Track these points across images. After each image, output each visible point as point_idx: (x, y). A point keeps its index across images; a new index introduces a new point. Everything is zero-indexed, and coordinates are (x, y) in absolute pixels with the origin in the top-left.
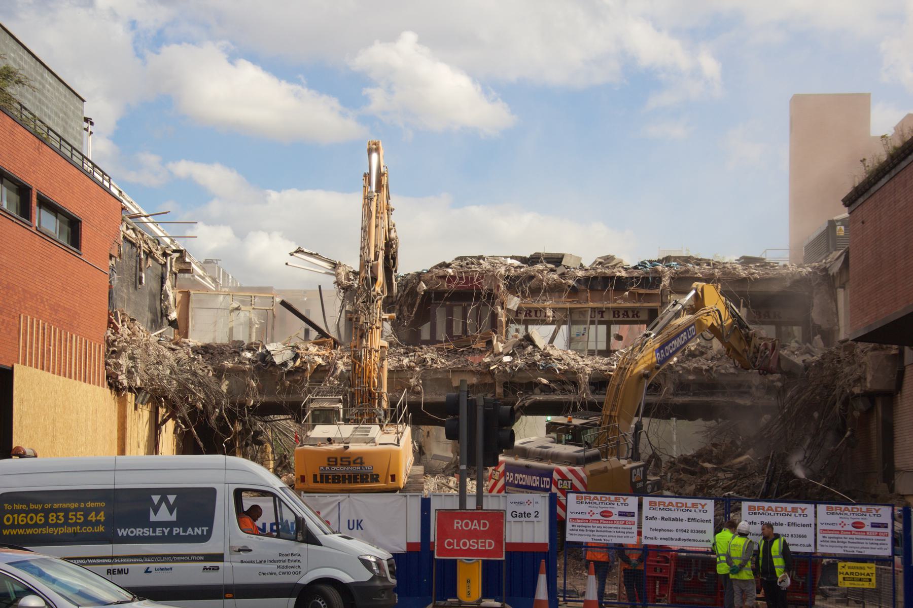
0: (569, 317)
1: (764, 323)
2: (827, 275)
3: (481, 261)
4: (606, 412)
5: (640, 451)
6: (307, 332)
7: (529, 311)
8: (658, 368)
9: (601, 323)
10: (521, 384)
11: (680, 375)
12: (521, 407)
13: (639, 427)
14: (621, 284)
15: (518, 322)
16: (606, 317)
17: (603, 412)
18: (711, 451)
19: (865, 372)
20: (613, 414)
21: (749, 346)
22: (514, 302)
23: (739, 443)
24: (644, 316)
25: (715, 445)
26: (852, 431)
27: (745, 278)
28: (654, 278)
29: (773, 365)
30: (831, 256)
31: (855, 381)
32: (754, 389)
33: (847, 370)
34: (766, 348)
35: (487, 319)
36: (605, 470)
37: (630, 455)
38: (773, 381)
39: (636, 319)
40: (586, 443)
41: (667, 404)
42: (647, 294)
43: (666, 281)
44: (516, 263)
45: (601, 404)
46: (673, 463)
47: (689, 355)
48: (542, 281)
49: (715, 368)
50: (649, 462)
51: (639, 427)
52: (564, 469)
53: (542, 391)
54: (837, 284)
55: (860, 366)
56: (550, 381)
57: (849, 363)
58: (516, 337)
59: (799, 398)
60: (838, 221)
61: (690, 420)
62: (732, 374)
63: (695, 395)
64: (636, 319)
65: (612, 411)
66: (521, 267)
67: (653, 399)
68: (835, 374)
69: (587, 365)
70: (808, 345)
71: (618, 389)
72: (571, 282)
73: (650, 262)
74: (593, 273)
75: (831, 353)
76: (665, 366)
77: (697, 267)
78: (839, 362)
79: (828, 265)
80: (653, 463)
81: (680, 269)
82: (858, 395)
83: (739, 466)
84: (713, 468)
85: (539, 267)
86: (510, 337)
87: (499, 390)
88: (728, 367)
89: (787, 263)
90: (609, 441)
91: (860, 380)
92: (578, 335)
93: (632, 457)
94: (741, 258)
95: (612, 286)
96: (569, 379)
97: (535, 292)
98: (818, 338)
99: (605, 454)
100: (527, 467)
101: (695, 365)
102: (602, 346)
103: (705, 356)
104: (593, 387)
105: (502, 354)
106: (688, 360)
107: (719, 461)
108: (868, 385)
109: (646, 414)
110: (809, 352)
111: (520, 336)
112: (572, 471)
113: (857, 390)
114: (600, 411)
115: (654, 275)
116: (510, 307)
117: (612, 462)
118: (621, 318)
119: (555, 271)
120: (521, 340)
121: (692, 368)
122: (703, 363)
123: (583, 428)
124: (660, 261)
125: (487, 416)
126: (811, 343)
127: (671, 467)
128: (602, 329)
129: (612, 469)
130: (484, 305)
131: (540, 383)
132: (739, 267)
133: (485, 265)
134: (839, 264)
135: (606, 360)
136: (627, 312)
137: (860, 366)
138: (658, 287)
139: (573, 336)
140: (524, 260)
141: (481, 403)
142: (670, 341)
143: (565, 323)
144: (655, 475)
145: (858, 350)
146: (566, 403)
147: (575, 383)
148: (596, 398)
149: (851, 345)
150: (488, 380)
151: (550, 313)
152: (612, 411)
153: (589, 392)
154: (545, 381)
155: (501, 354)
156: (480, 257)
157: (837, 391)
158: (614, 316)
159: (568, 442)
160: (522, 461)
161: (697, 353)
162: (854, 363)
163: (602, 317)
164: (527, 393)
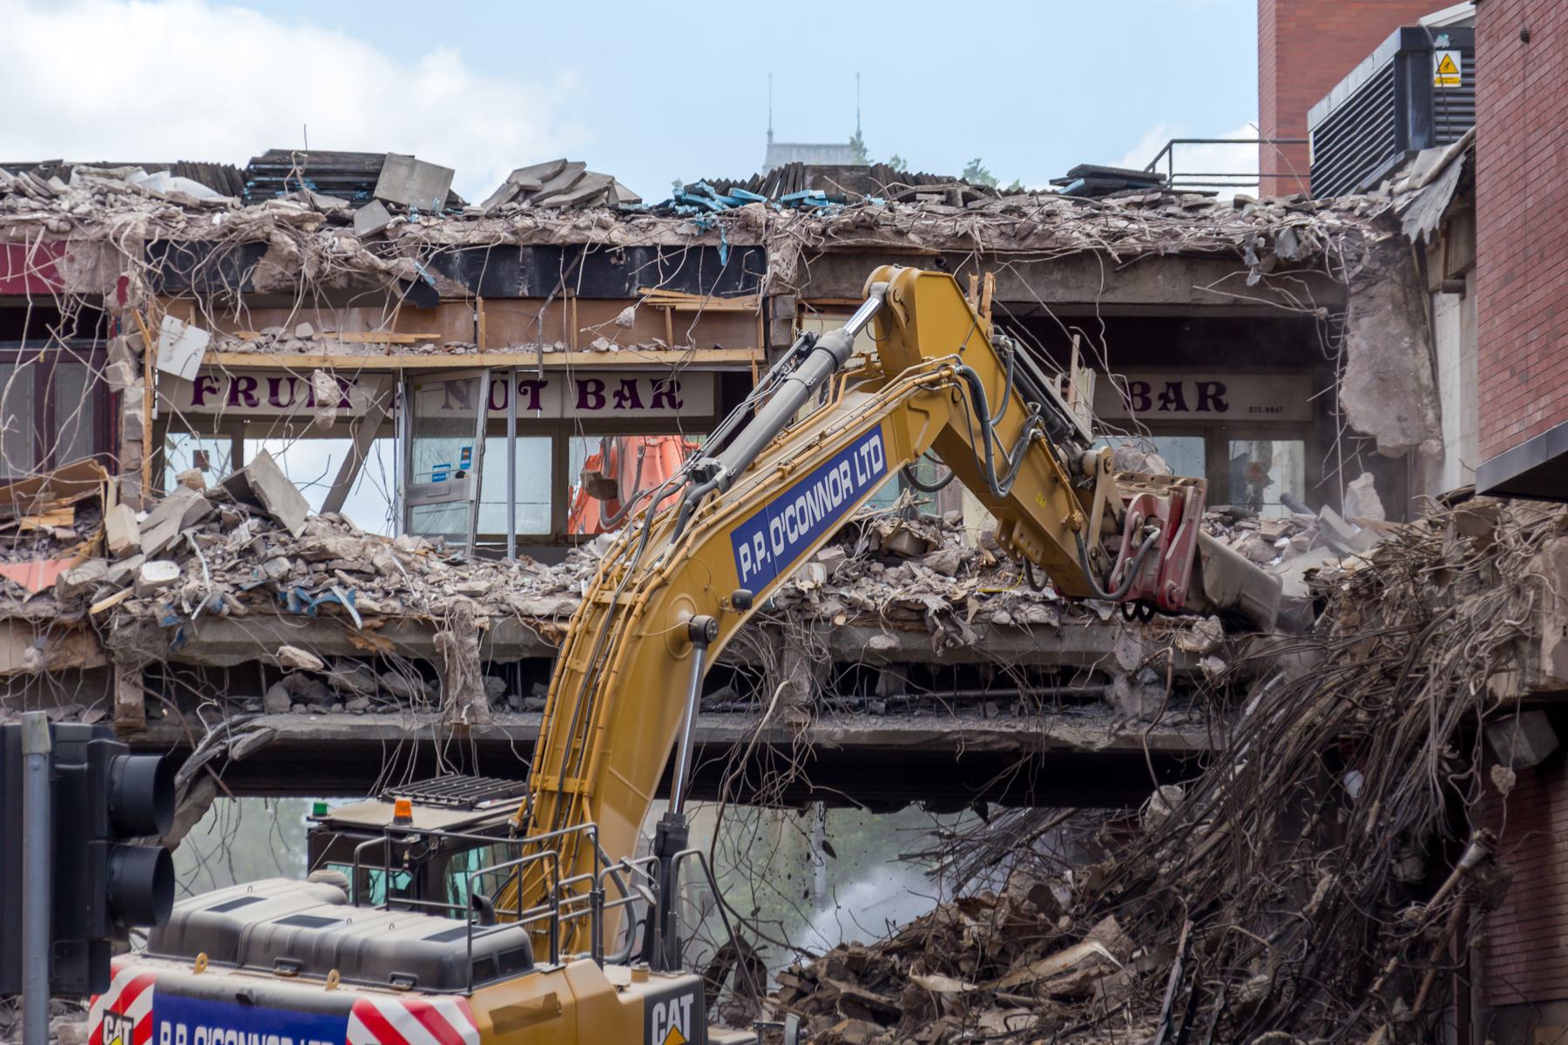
0: (410, 402)
1: (1160, 428)
2: (1398, 241)
3: (56, 184)
4: (543, 778)
5: (683, 932)
6: (1359, 513)
7: (244, 383)
8: (744, 604)
9: (528, 428)
10: (216, 673)
11: (838, 632)
12: (216, 763)
13: (669, 841)
14: (597, 275)
15: (203, 425)
16: (550, 408)
17: (535, 780)
18: (957, 929)
19: (1534, 616)
20: (572, 785)
21: (1087, 510)
22: (184, 346)
23: (1062, 896)
24: (699, 403)
25: (969, 906)
26: (1487, 841)
27: (1088, 254)
28: (736, 251)
29: (1177, 584)
30: (1412, 168)
31: (1497, 652)
32: (1120, 687)
33: (1469, 607)
34: (1150, 517)
35: (76, 415)
36: (550, 1008)
37: (638, 947)
38: (1194, 655)
39: (666, 412)
40: (477, 903)
41: (786, 748)
42: (709, 316)
43: (781, 261)
44: (198, 191)
45: (527, 748)
46: (809, 979)
47: (871, 555)
48: (294, 260)
49: (973, 606)
50: (715, 974)
51: (669, 841)
52: (392, 1005)
53: (297, 698)
54: (1436, 276)
55: (1517, 592)
56: (330, 660)
57: (1479, 584)
58: (194, 484)
59: (1289, 720)
60: (1436, 31)
61: (877, 808)
62: (1035, 625)
63: (894, 708)
64: (666, 412)
65: (566, 774)
66: (212, 208)
67: (731, 727)
68: (1422, 623)
69: (476, 598)
70: (1327, 512)
71: (591, 687)
72: (410, 265)
73: (724, 187)
74: (500, 231)
75: (1411, 541)
76: (774, 592)
77: (906, 209)
78: (1439, 577)
79: (1400, 203)
80: (731, 980)
81: (837, 215)
82: (1509, 706)
83: (1062, 985)
84: (962, 995)
85: (288, 205)
86: (170, 484)
87: (128, 695)
88: (1022, 601)
89: (1253, 193)
90: (560, 893)
91: (1518, 644)
92: (439, 477)
93: (646, 954)
94: (1074, 174)
95: (571, 282)
96: (406, 657)
97: (270, 304)
98: (1363, 485)
99: (550, 942)
100: (243, 999)
101: (897, 593)
102: (536, 521)
103: (935, 557)
104: (499, 685)
105: (148, 550)
106: (866, 572)
107: (956, 963)
108: (1548, 666)
109: (704, 785)
110: (1327, 539)
111: (211, 481)
112: (420, 1013)
113: (1506, 686)
114: (521, 773)
115: (738, 239)
116: (173, 368)
117: (578, 978)
118: (609, 411)
119: (345, 222)
120: (216, 499)
121: (882, 604)
122: (925, 586)
123: (456, 845)
124: (755, 185)
125: (64, 790)
126: (1337, 509)
127: (801, 994)
128: (536, 452)
129: (576, 1004)
130: (66, 359)
131: (290, 667)
132: (1067, 209)
133: (77, 198)
134: (1441, 197)
135: (549, 574)
136: (631, 385)
137: (1517, 592)
138: (750, 285)
139: (422, 479)
140: (224, 179)
141: (39, 744)
142: (789, 497)
143: (387, 428)
144: (737, 1022)
145: (1511, 532)
146: (392, 745)
147: (428, 669)
148: (510, 724)
149: (1482, 511)
150: (84, 655)
151: (325, 387)
152: (566, 774)
153: (481, 701)
154: (307, 660)
155: (131, 551)
156: (58, 169)
157: (1432, 692)
158: (582, 404)
159: (395, 900)
160: (221, 979)
161: (904, 544)
162: (1496, 579)
163: (535, 404)
164: (238, 706)
